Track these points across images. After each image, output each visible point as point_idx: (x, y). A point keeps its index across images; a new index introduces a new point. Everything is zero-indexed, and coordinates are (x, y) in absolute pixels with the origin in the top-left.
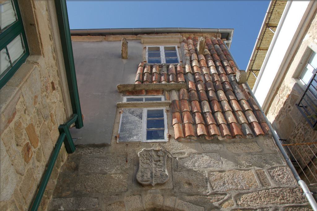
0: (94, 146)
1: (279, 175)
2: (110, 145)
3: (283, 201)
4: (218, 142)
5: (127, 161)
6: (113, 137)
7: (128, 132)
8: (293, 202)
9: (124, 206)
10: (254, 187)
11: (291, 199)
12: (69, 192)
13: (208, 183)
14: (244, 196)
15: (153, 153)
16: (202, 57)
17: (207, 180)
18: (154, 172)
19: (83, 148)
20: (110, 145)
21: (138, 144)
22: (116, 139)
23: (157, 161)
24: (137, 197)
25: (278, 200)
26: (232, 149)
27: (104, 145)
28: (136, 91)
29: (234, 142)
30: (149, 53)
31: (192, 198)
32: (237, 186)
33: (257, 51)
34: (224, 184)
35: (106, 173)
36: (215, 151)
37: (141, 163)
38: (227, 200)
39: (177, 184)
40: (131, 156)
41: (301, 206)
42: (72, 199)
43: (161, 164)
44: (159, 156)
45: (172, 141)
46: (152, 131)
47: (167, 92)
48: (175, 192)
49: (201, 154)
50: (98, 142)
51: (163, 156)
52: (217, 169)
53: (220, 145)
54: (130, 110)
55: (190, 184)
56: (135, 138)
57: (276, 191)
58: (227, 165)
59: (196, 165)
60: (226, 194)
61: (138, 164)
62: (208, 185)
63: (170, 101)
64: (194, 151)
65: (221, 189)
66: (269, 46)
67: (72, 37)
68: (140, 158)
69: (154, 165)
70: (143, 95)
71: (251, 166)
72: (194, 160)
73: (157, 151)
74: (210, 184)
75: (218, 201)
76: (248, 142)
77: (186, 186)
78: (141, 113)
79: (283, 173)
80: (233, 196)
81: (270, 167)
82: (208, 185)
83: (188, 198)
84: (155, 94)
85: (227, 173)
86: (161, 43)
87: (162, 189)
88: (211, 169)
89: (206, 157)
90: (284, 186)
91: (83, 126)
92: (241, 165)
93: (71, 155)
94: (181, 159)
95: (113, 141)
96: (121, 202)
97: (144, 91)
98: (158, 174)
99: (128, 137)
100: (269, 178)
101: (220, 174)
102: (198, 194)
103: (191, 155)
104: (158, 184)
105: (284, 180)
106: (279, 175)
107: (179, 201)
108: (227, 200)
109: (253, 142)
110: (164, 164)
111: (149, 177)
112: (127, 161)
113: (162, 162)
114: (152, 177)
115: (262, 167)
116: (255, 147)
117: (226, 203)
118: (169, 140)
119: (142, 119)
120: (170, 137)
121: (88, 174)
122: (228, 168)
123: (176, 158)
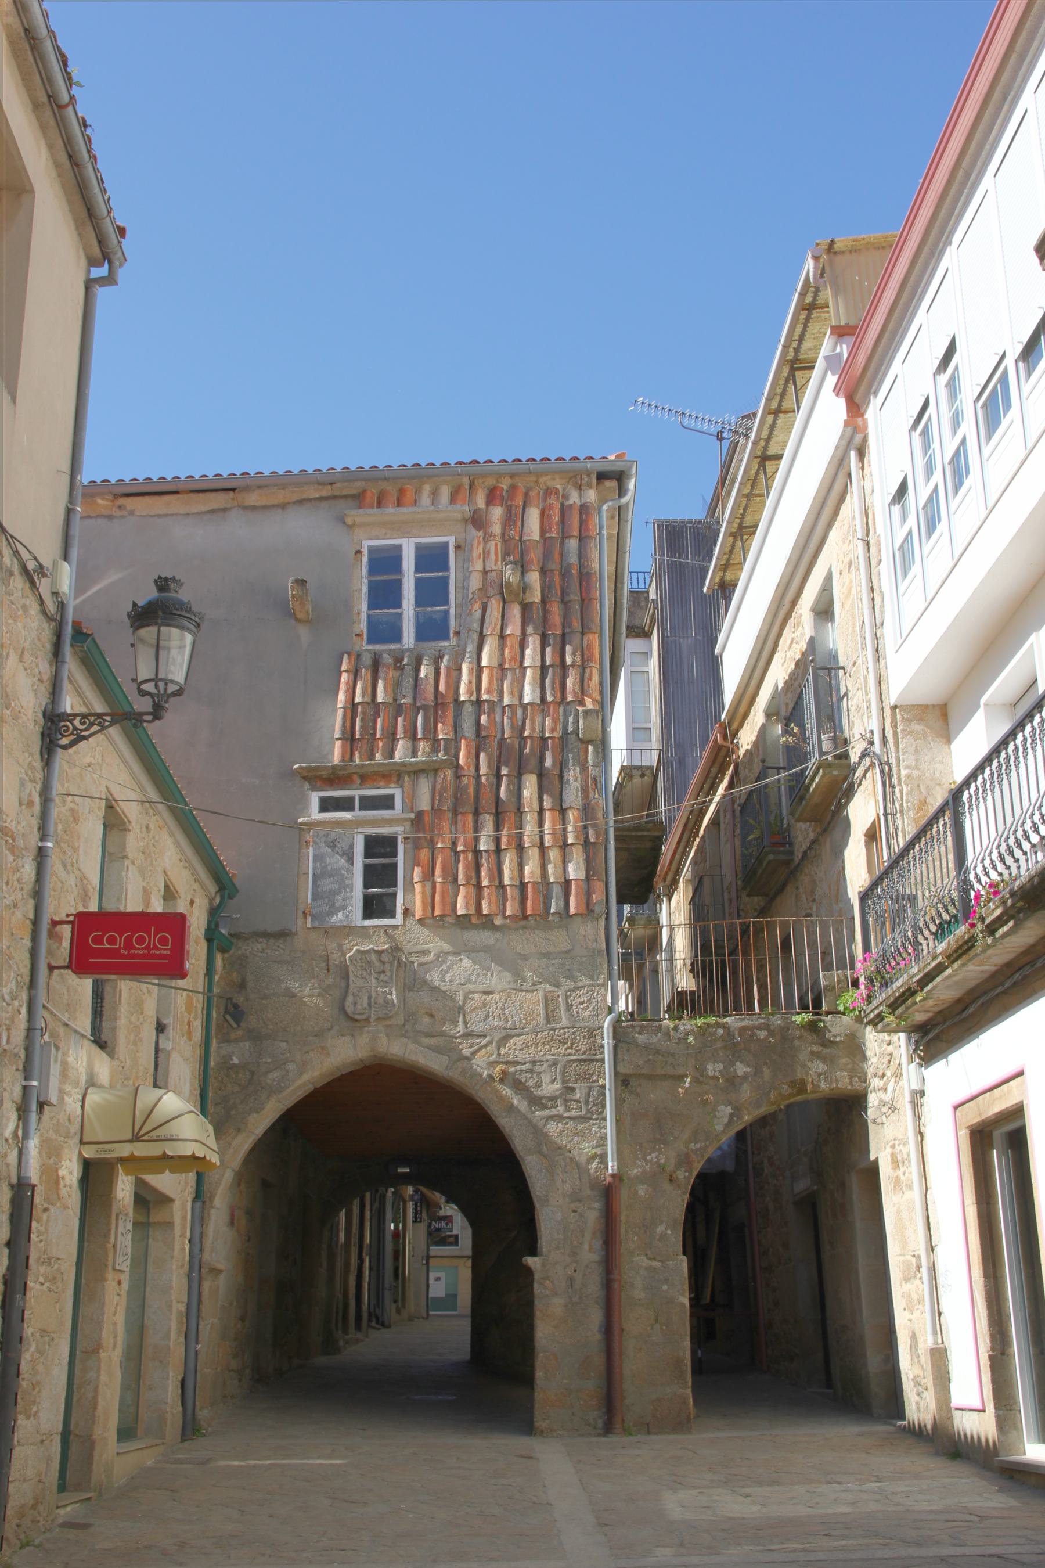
0: (266, 935)
1: (582, 1003)
2: (295, 934)
3: (569, 1051)
4: (495, 928)
5: (328, 970)
6: (300, 914)
7: (326, 901)
8: (584, 1053)
9: (328, 1054)
10: (533, 1023)
11: (583, 1048)
12: (240, 1032)
13: (461, 1016)
14: (512, 1041)
15: (373, 957)
16: (515, 611)
17: (461, 1009)
18: (374, 995)
19: (246, 939)
20: (295, 934)
21: (347, 930)
22: (306, 918)
23: (379, 973)
24: (347, 1039)
25: (562, 1050)
26: (520, 942)
27: (283, 934)
28: (338, 778)
29: (524, 927)
30: (370, 582)
31: (432, 1041)
32: (507, 1021)
33: (770, 419)
34: (487, 1016)
35: (294, 996)
36: (486, 949)
37: (352, 978)
38: (485, 1046)
39: (411, 1017)
40: (335, 959)
41: (593, 1061)
42: (247, 1044)
43: (386, 978)
44: (384, 963)
45: (411, 923)
46: (373, 895)
47: (409, 776)
48: (406, 1031)
49: (459, 954)
50: (272, 928)
51: (393, 959)
52: (481, 988)
53: (498, 935)
54: (327, 835)
55: (432, 1016)
56: (340, 914)
57: (565, 1033)
58: (498, 979)
59: (447, 978)
60: (485, 1036)
61: (346, 977)
62: (461, 1019)
63: (412, 816)
64: (446, 947)
65: (477, 1027)
66: (784, 449)
67: (192, 1176)
68: (351, 968)
69: (374, 981)
70: (354, 786)
71: (541, 983)
72: (444, 967)
73: (379, 953)
74: (464, 1017)
75: (471, 1047)
76: (551, 928)
77: (426, 1020)
78: (352, 847)
79: (590, 1000)
80: (496, 1039)
81: (572, 985)
82: (461, 1019)
83: (426, 1041)
84: (382, 784)
85: (496, 996)
86: (403, 528)
87: (387, 1026)
88: (471, 986)
89: (467, 962)
90: (582, 1024)
91: (237, 891)
92: (524, 979)
93: (226, 955)
94: (421, 964)
95: (300, 922)
96: (323, 1048)
97: (356, 778)
98: (381, 1000)
99: (328, 915)
100: (562, 1008)
101: (484, 997)
102: (443, 1034)
103: (441, 957)
104: (378, 1019)
105: (587, 1013)
106: (582, 1003)
107: (411, 1046)
108: (485, 1046)
109: (560, 927)
110: (391, 978)
111: (365, 1005)
112: (328, 970)
113: (388, 974)
114: (369, 1004)
115: (557, 985)
116: (559, 940)
117: (484, 1050)
118: (405, 920)
119: (352, 864)
120: (407, 912)
121: (265, 997)
122: (499, 987)
123: (413, 963)
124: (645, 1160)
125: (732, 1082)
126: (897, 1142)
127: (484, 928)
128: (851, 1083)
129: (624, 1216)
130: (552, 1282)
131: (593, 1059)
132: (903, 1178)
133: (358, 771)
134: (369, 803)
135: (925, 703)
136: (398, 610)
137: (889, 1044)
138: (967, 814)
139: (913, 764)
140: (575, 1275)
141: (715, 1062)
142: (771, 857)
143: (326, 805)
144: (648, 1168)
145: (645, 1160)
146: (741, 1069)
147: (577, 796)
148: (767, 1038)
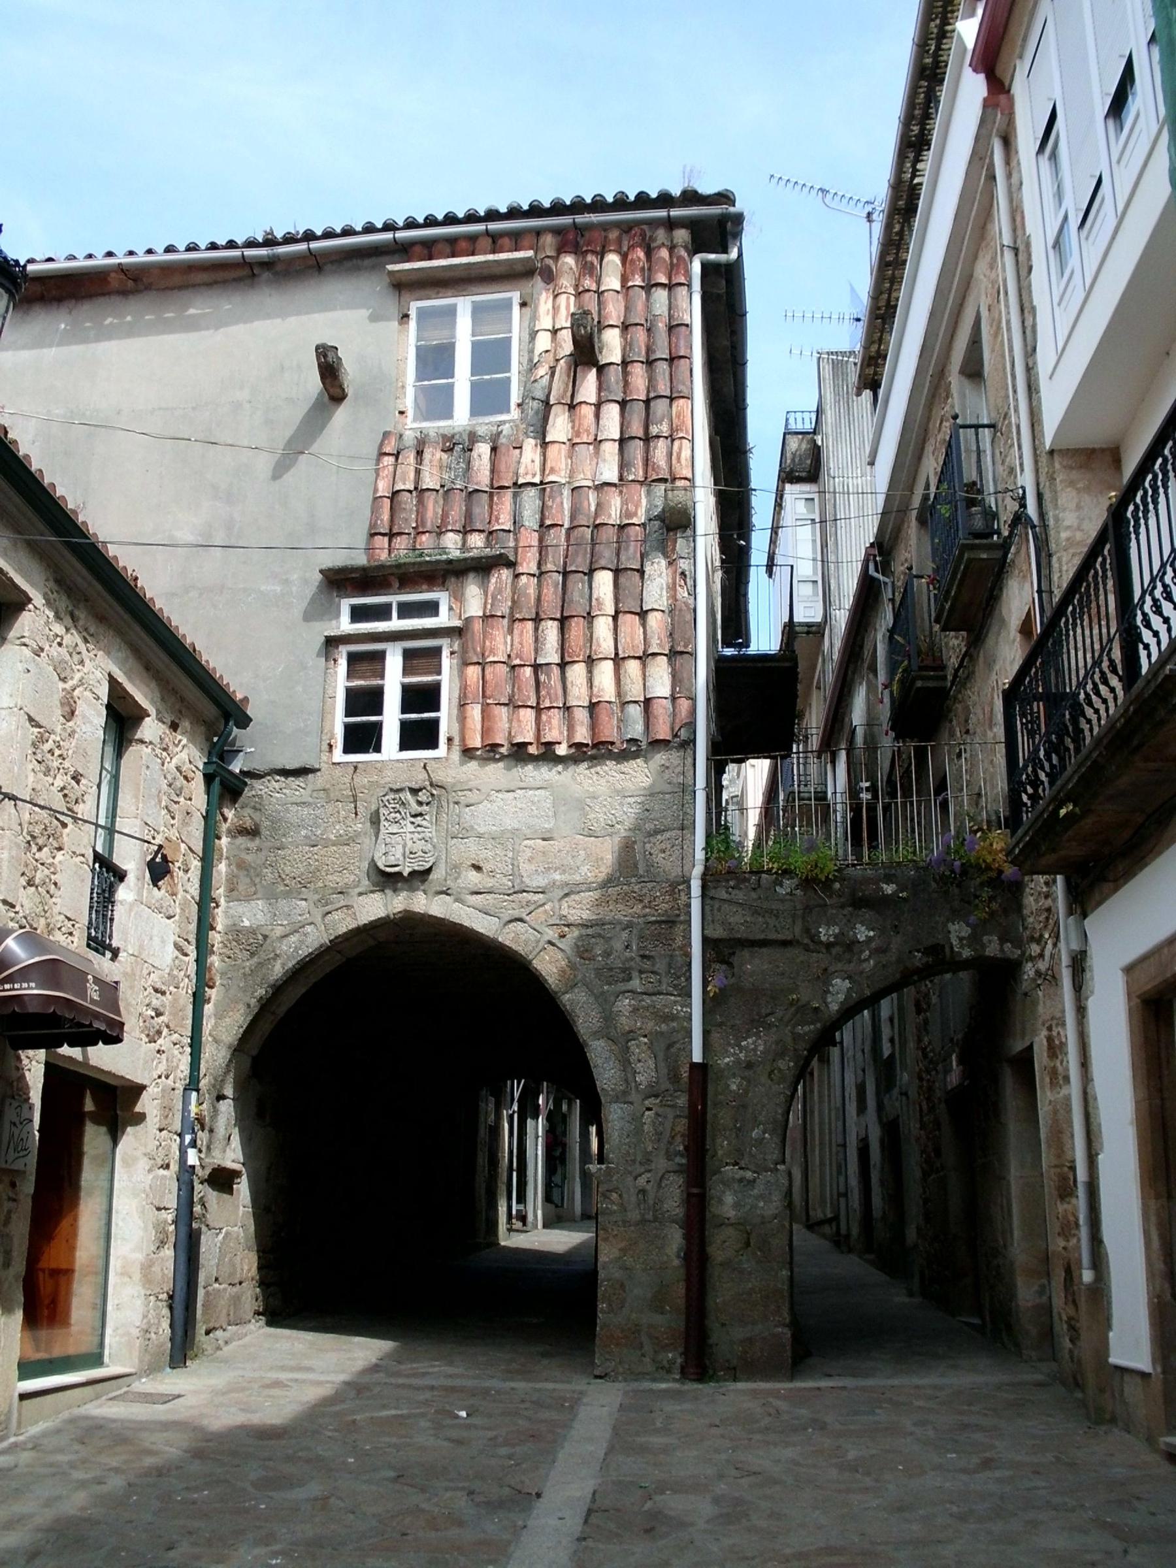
84: (425, 587)
112: (356, 814)
124: (739, 1046)
125: (850, 946)
126: (1055, 1022)
127: (544, 760)
128: (1002, 950)
129: (721, 1117)
130: (620, 1196)
131: (675, 921)
132: (1060, 1069)
133: (395, 571)
134: (407, 610)
135: (1091, 446)
136: (450, 380)
137: (1046, 897)
138: (1133, 536)
139: (1075, 524)
140: (648, 1187)
141: (828, 925)
142: (919, 684)
143: (359, 614)
144: (742, 1056)
145: (739, 1046)
146: (863, 933)
147: (661, 596)
148: (895, 893)
